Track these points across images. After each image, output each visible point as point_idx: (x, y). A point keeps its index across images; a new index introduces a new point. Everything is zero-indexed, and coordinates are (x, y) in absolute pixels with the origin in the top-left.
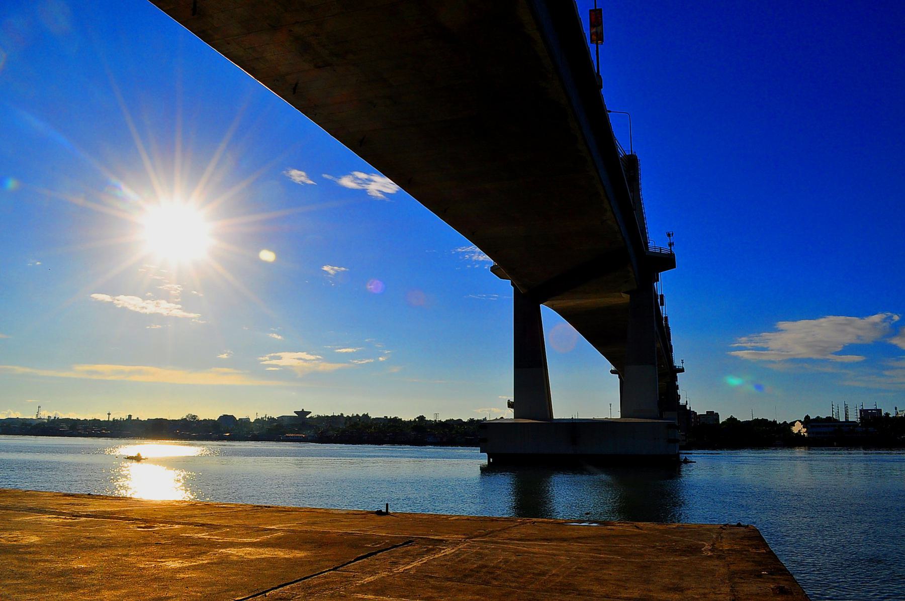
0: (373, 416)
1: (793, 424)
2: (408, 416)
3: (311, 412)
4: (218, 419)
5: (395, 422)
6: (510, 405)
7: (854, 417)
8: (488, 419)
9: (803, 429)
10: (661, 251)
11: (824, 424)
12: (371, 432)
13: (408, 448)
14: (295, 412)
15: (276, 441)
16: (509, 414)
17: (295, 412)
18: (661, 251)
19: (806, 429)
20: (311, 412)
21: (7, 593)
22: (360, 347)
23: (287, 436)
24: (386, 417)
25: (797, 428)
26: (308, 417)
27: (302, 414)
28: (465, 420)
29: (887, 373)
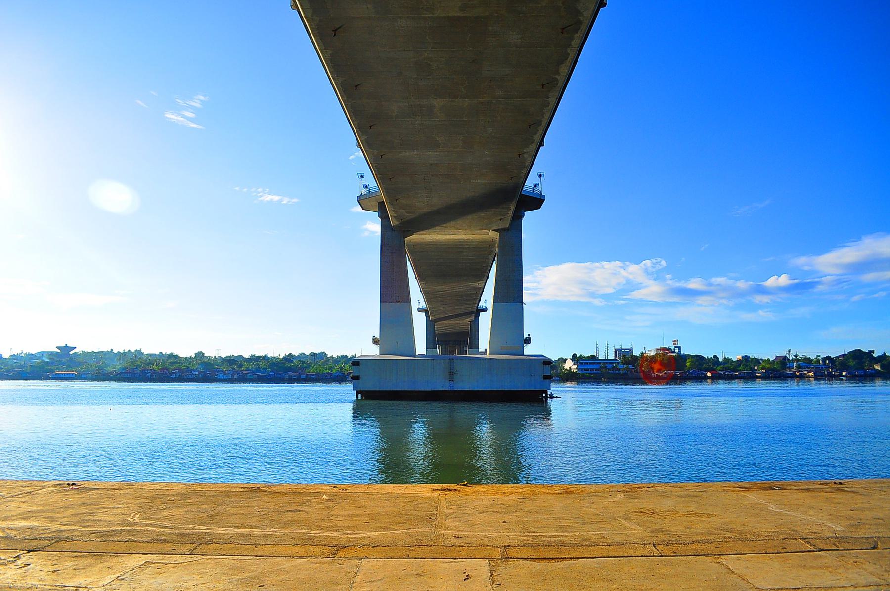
0: (146, 351)
1: (564, 361)
2: (186, 352)
3: (75, 348)
4: (635, 356)
5: (319, 358)
6: (375, 341)
7: (611, 356)
8: (357, 356)
9: (573, 366)
10: (533, 191)
11: (591, 361)
12: (153, 368)
13: (309, 387)
14: (57, 347)
15: (44, 380)
16: (373, 351)
17: (57, 347)
18: (533, 191)
19: (576, 366)
20: (75, 348)
21: (794, 515)
22: (759, 285)
23: (56, 374)
24: (161, 353)
25: (569, 365)
26: (71, 353)
27: (66, 349)
28: (247, 356)
29: (628, 318)
